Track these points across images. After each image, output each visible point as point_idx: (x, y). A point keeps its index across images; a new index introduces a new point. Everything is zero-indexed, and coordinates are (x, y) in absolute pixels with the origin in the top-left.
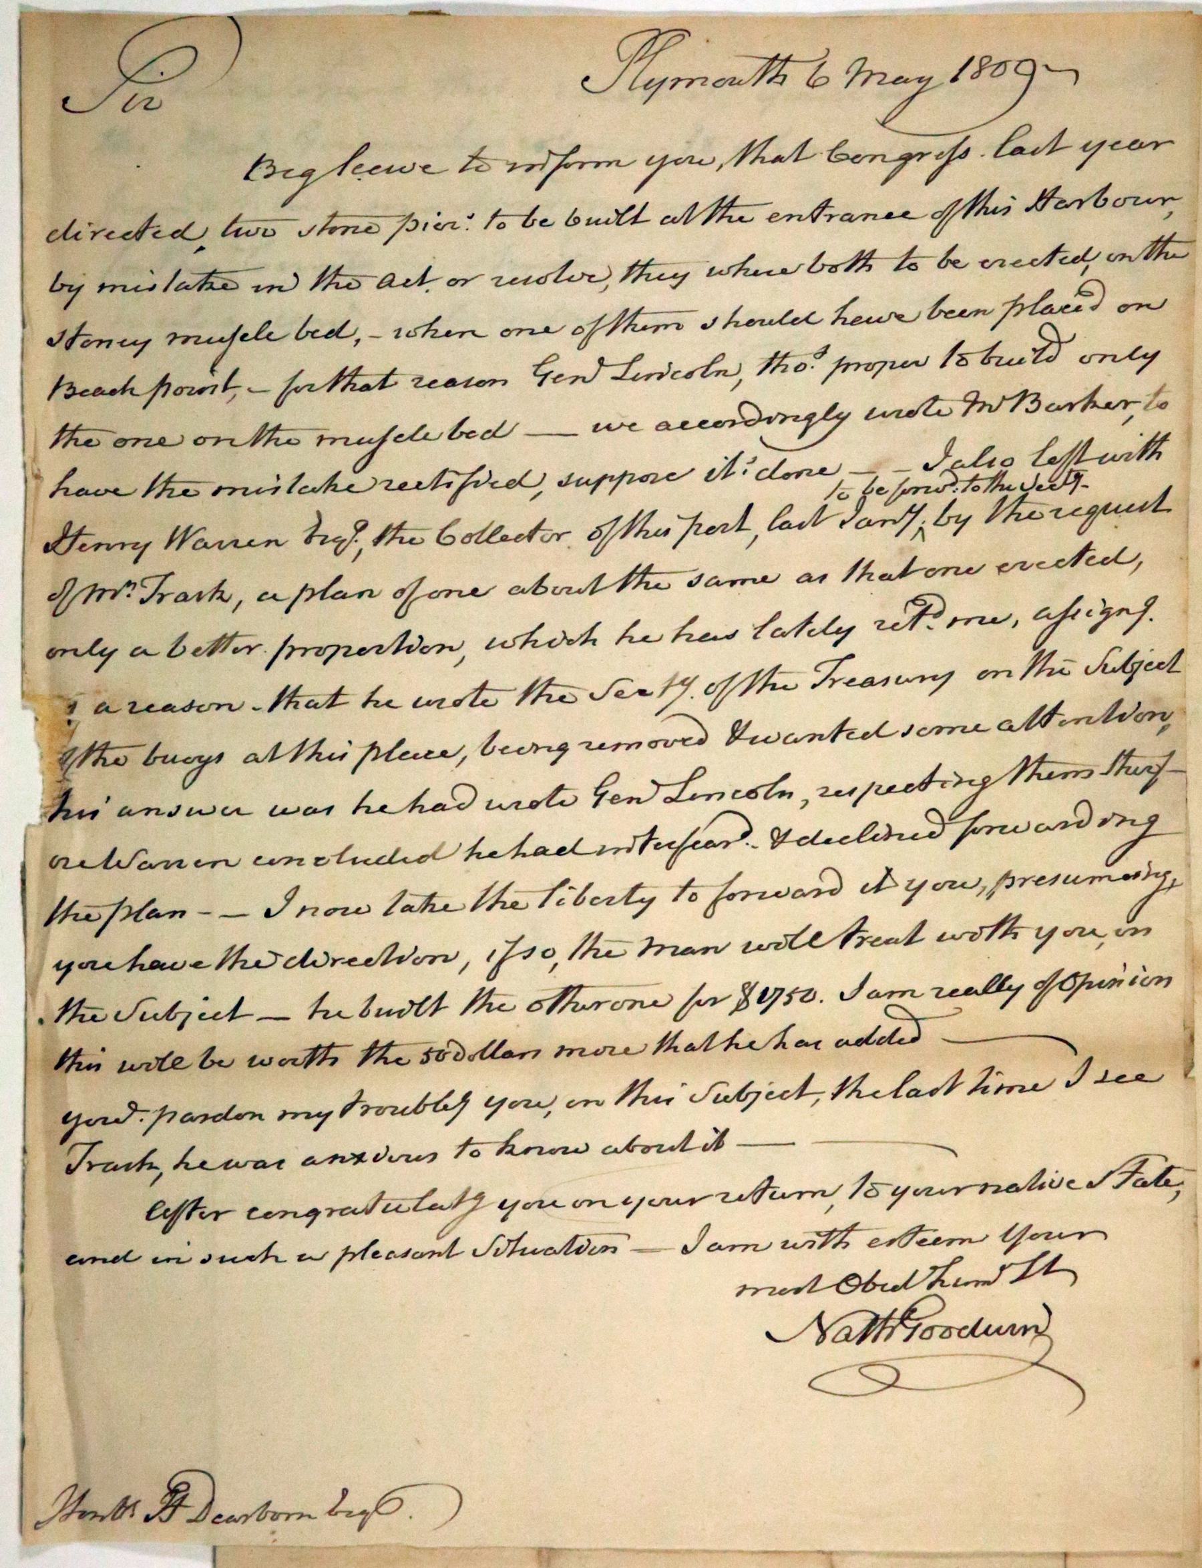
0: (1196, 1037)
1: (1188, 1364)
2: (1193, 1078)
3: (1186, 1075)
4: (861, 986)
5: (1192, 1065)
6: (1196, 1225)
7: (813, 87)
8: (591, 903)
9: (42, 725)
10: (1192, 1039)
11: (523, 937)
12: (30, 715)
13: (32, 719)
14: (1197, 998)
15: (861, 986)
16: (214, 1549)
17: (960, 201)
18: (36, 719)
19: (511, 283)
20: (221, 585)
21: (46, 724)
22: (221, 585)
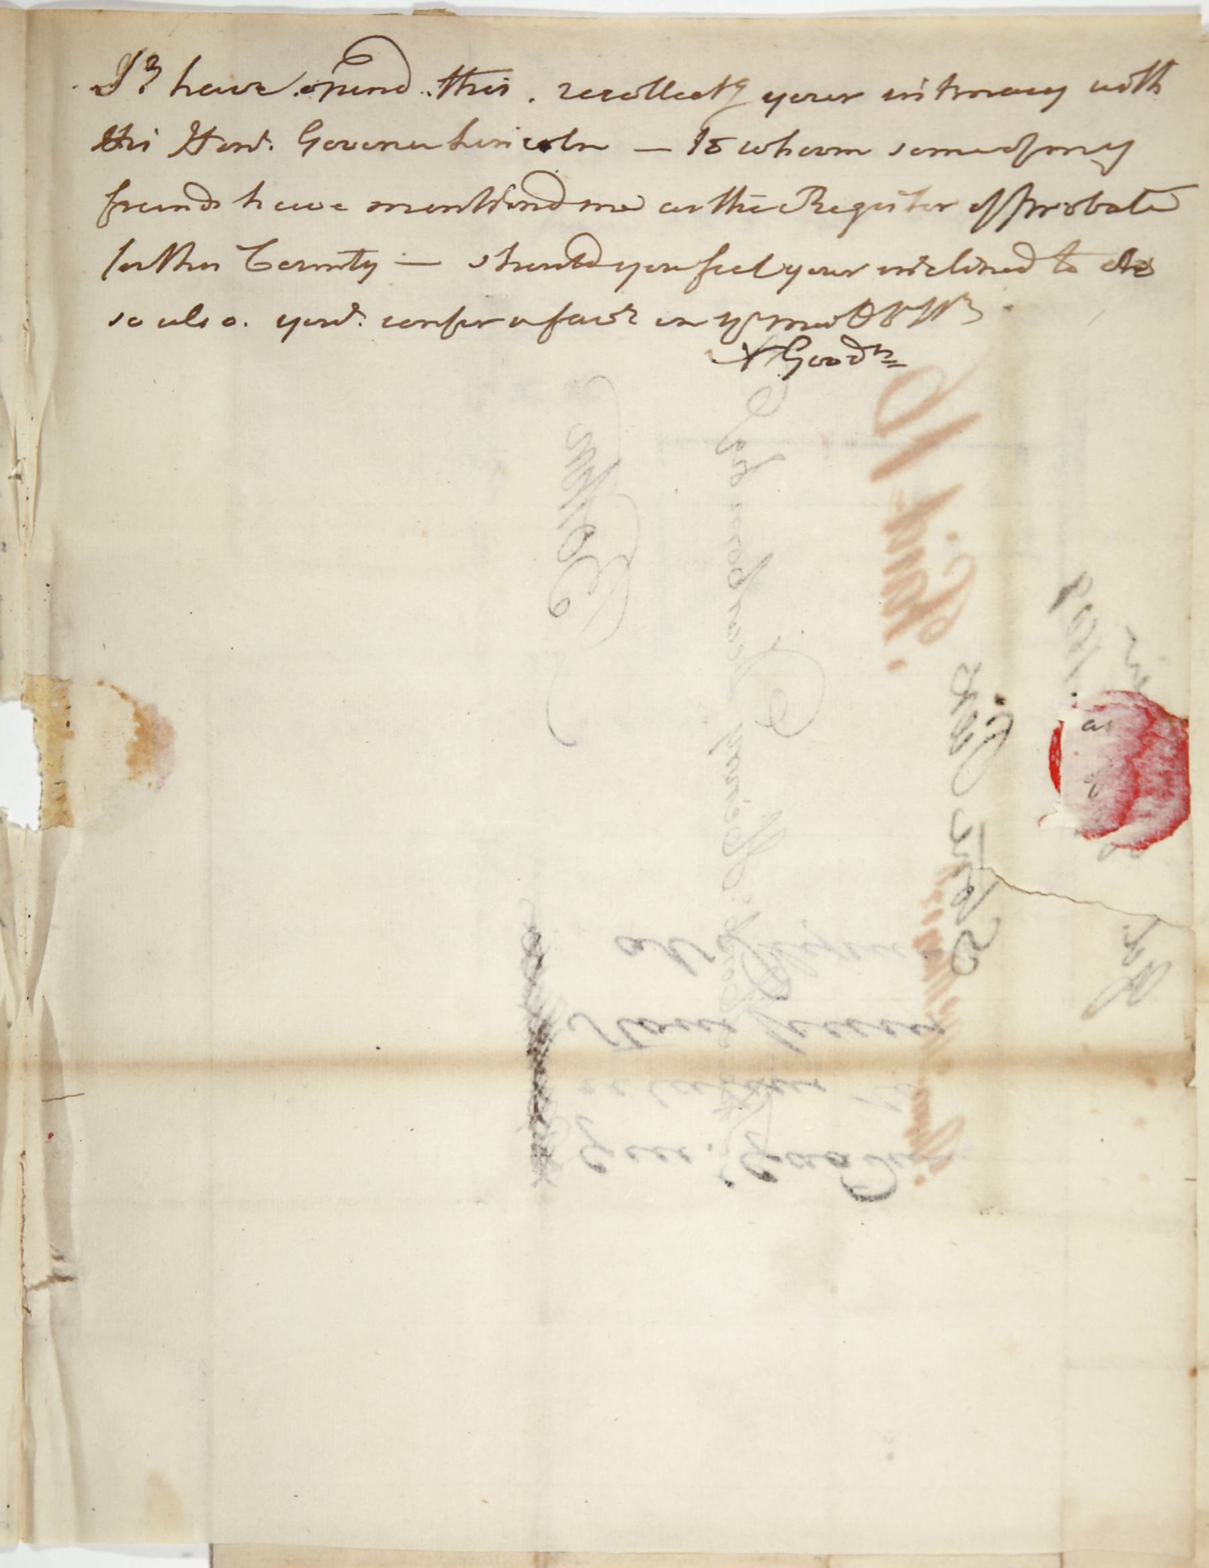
0: (1197, 1046)
1: (1185, 1373)
2: (1194, 1088)
3: (1187, 1085)
4: (982, 836)
5: (1193, 1074)
6: (1195, 1234)
7: (818, 188)
8: (810, 365)
9: (41, 727)
10: (1193, 1048)
11: (797, 132)
12: (29, 716)
13: (32, 721)
14: (1199, 1007)
15: (982, 836)
16: (211, 1546)
17: (1001, 192)
18: (35, 720)
19: (582, 96)
20: (256, 191)
21: (45, 726)
22: (256, 191)
